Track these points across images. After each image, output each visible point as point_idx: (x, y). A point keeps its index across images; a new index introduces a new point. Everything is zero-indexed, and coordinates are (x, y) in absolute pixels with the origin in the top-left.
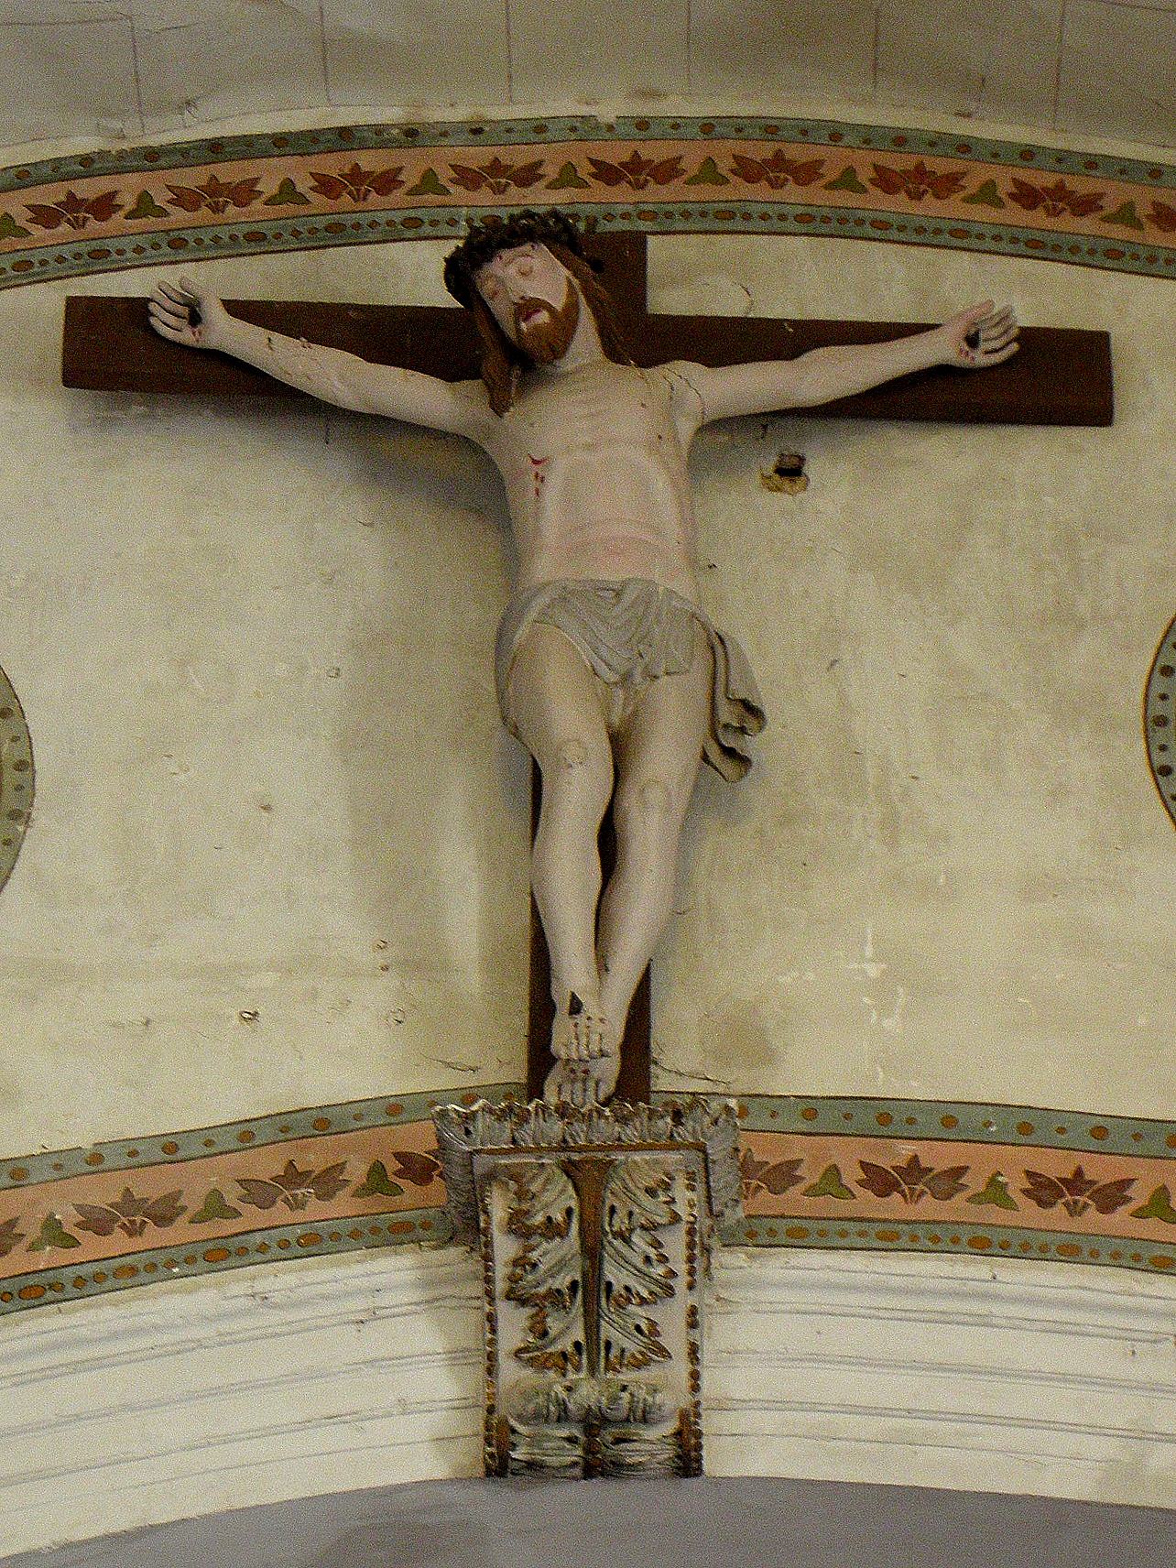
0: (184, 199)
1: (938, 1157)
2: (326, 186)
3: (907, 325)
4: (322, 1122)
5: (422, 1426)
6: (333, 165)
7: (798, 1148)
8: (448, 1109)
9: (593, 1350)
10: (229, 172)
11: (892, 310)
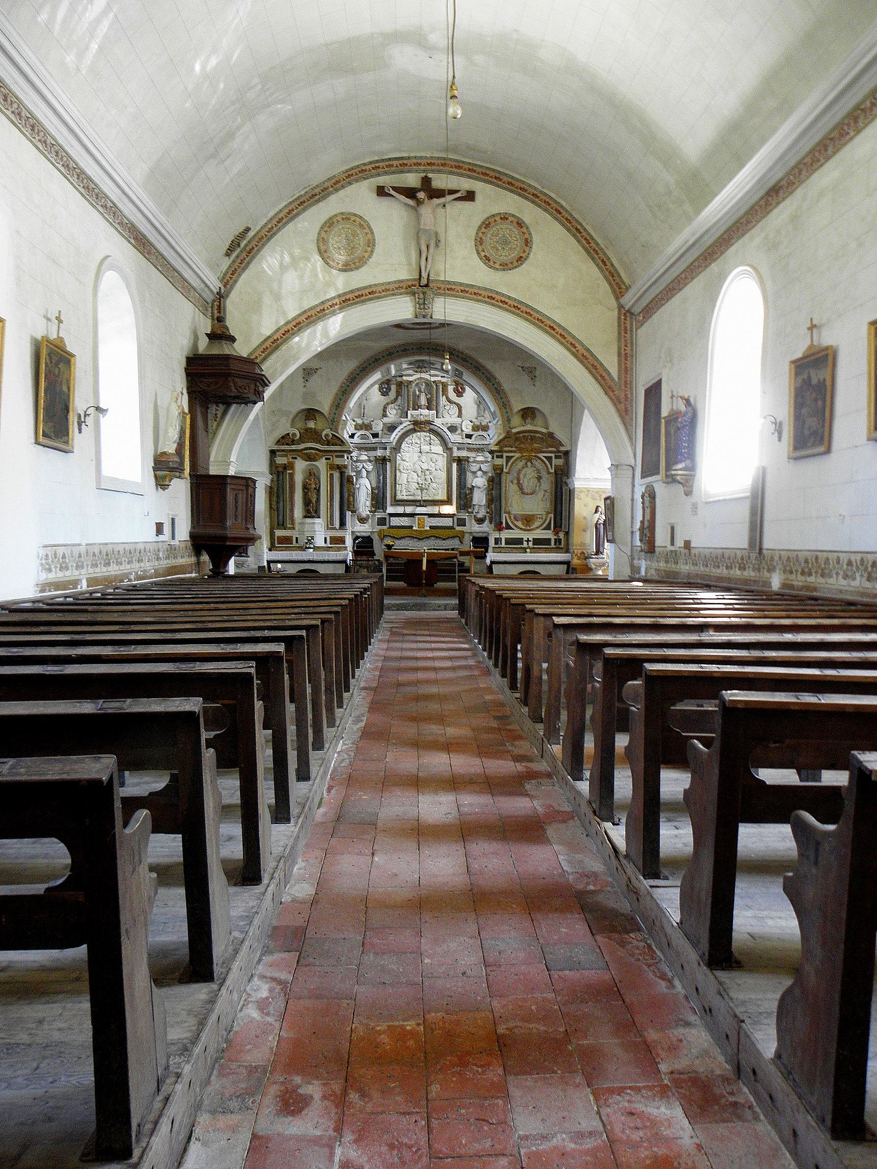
0: (387, 166)
1: (453, 287)
2: (401, 165)
3: (466, 200)
4: (402, 281)
5: (410, 313)
6: (401, 162)
7: (441, 285)
8: (188, 1062)
9: (424, 308)
10: (391, 163)
11: (455, 188)
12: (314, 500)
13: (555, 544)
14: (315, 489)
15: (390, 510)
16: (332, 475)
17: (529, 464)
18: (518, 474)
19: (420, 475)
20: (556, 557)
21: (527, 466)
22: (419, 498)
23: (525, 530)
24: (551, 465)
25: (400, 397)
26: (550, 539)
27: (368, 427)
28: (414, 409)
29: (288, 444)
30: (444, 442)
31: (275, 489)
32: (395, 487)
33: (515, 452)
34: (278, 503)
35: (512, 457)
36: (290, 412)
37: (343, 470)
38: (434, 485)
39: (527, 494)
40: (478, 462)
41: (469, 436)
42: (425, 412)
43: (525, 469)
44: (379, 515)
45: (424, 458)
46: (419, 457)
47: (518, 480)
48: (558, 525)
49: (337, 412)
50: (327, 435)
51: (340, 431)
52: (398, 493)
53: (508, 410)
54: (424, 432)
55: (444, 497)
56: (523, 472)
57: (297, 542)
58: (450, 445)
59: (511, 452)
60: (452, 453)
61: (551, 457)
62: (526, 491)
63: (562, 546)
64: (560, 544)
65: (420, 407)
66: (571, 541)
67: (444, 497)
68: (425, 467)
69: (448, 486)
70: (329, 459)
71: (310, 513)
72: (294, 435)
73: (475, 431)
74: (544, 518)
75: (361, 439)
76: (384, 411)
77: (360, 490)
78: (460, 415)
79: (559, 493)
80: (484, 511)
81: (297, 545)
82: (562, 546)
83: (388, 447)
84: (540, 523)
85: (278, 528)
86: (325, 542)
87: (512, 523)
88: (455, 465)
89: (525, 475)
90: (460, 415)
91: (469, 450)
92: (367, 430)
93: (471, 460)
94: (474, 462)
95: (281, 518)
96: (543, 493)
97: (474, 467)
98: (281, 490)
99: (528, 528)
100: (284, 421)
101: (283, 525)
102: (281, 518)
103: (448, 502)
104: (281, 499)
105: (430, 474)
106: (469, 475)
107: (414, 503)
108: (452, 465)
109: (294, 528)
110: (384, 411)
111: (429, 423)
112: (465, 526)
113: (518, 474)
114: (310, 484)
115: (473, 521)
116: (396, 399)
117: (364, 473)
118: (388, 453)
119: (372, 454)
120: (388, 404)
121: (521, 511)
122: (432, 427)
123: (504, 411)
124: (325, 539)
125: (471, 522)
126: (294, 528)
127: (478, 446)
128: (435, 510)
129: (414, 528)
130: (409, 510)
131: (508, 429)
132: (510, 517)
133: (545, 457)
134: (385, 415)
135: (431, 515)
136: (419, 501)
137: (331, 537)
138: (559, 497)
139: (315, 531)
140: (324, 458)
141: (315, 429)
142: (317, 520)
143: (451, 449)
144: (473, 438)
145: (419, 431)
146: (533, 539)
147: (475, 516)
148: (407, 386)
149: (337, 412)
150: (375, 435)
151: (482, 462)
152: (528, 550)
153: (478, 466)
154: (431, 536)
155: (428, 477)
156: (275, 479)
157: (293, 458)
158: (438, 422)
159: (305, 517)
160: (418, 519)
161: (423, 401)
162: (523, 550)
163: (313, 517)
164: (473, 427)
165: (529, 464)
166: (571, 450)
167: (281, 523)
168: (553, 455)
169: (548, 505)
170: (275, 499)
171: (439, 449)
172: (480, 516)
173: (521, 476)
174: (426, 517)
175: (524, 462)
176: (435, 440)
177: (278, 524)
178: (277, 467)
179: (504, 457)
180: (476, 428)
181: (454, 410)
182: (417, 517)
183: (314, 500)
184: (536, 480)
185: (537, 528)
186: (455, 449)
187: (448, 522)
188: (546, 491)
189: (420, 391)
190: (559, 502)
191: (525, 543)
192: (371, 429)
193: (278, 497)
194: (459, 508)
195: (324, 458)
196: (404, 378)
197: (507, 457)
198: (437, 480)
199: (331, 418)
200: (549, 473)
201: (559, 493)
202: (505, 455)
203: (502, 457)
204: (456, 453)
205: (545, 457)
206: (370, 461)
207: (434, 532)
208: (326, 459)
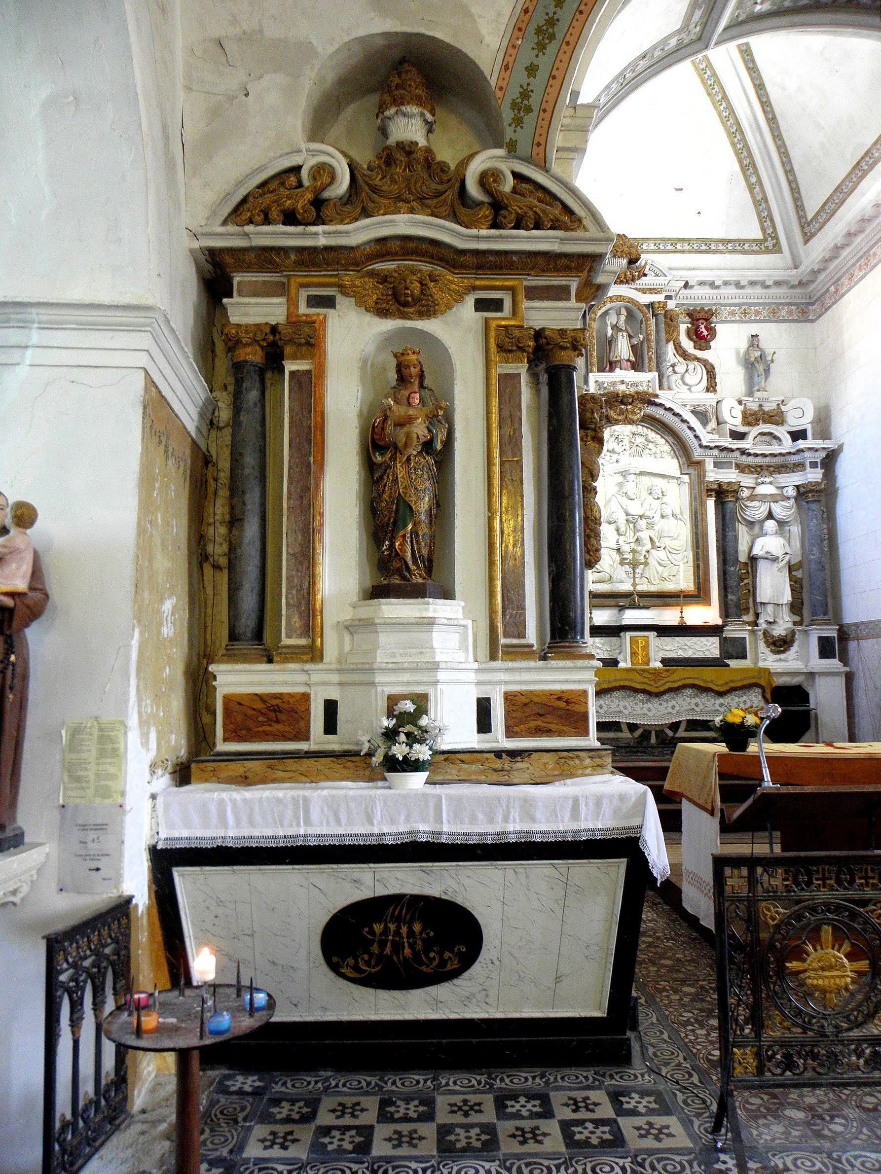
12: (423, 505)
14: (428, 446)
16: (509, 382)
19: (622, 529)
22: (626, 587)
28: (601, 370)
29: (290, 218)
30: (681, 448)
31: (225, 464)
34: (235, 521)
36: (305, 50)
37: (563, 357)
38: (661, 555)
40: (763, 498)
41: (738, 436)
42: (631, 376)
45: (630, 488)
46: (620, 485)
49: (544, 62)
50: (486, 179)
51: (556, 168)
54: (631, 422)
55: (685, 582)
57: (330, 727)
58: (697, 454)
60: (701, 475)
65: (612, 366)
67: (685, 582)
68: (635, 509)
69: (696, 558)
70: (496, 305)
71: (403, 570)
72: (324, 172)
73: (749, 424)
78: (711, 387)
80: (787, 618)
81: (333, 743)
85: (231, 657)
86: (484, 724)
88: (711, 503)
90: (711, 387)
91: (741, 468)
93: (746, 493)
94: (752, 498)
95: (248, 601)
97: (757, 511)
98: (250, 460)
100: (273, 98)
101: (258, 635)
102: (248, 601)
103: (700, 595)
104: (252, 499)
105: (650, 526)
106: (742, 531)
107: (612, 601)
108: (703, 504)
109: (314, 654)
111: (648, 400)
112: (744, 657)
114: (405, 422)
115: (762, 646)
122: (651, 410)
124: (484, 708)
125: (756, 647)
126: (314, 654)
127: (759, 460)
128: (669, 616)
129: (622, 665)
135: (664, 631)
136: (627, 595)
137: (509, 698)
139: (434, 667)
140: (470, 301)
141: (428, 150)
142: (437, 608)
143: (699, 464)
144: (751, 437)
145: (617, 422)
147: (766, 633)
149: (544, 62)
151: (774, 499)
153: (763, 510)
154: (684, 687)
155: (644, 535)
156: (224, 414)
157: (316, 301)
158: (664, 397)
159: (378, 592)
161: (623, 349)
163: (418, 592)
164: (744, 414)
167: (247, 623)
170: (219, 509)
171: (671, 465)
172: (779, 631)
174: (652, 635)
176: (661, 444)
177: (233, 637)
178: (233, 344)
180: (751, 418)
181: (697, 375)
182: (629, 635)
183: (423, 505)
186: (709, 465)
187: (709, 647)
193: (236, 490)
194: (726, 611)
195: (470, 301)
198: (666, 542)
199: (514, 93)
204: (713, 475)
207: (681, 675)
208: (481, 305)
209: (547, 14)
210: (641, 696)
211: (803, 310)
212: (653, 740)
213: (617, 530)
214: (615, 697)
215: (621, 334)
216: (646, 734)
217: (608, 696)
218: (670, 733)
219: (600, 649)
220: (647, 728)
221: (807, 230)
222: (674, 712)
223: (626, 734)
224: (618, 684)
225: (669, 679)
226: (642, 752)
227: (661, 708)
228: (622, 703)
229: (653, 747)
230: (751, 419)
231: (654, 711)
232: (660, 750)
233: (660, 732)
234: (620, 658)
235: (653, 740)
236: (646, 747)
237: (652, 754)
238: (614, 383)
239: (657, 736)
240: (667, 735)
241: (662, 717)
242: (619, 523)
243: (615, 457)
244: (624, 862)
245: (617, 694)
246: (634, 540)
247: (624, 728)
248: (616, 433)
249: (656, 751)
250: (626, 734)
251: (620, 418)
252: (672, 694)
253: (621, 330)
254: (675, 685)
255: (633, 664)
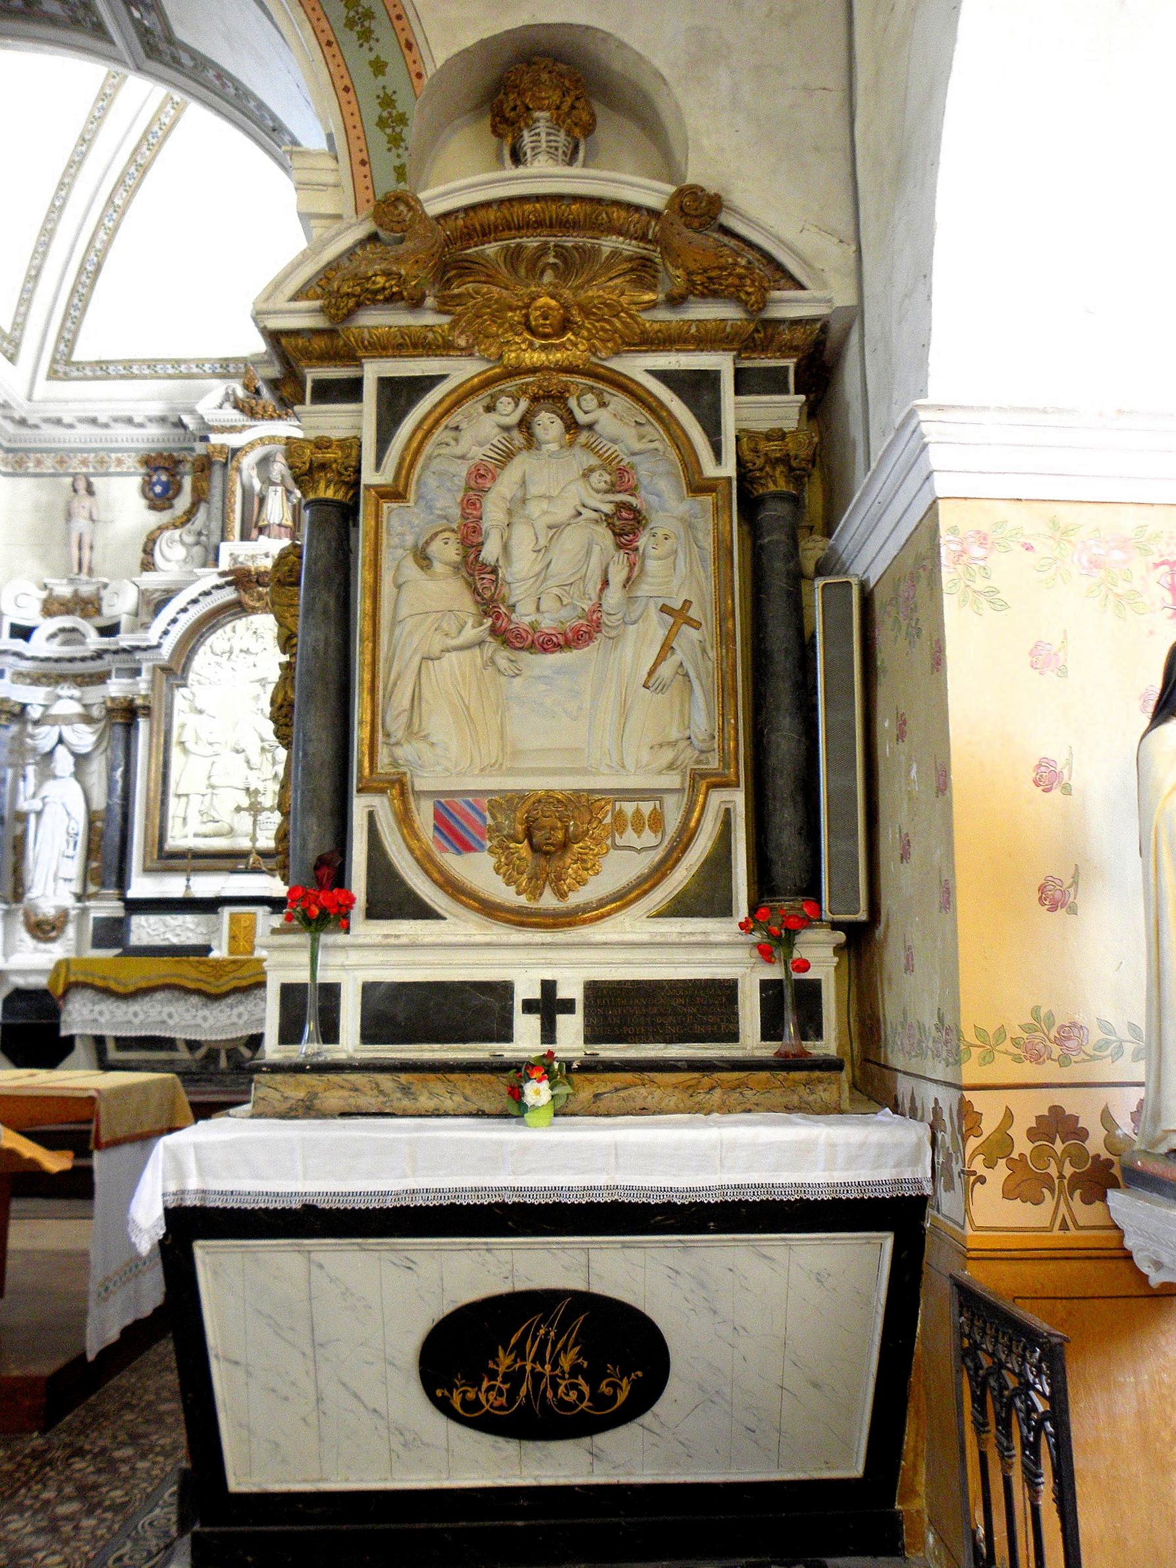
13: (770, 1030)
15: (141, 886)
17: (548, 425)
18: (473, 498)
20: (805, 1149)
21: (531, 442)
22: (244, 844)
23: (521, 919)
24: (713, 430)
25: (203, 508)
26: (726, 991)
27: (87, 606)
28: (245, 536)
32: (164, 803)
33: (444, 348)
35: (423, 385)
39: (548, 645)
43: (521, 464)
44: (107, 907)
47: (471, 540)
48: (787, 869)
52: (170, 832)
53: (386, 47)
56: (505, 485)
59: (418, 345)
61: (710, 379)
62: (524, 616)
63: (828, 1045)
64: (811, 1025)
66: (890, 1011)
74: (673, 822)
75: (65, 643)
76: (148, 551)
77: (45, 818)
79: (779, 637)
82: (828, 1045)
83: (145, 667)
84: (641, 865)
87: (427, 863)
89: (517, 506)
92: (85, 616)
96: (656, 628)
99: (549, 901)
107: (228, 863)
110: (148, 551)
113: (473, 498)
116: (190, 514)
117: (64, 762)
118: (142, 684)
119: (95, 694)
120: (161, 529)
121: (494, 768)
123: (359, 59)
129: (215, 954)
130: (206, 886)
131: (387, 184)
132: (404, 819)
133: (663, 376)
134: (148, 565)
138: (783, 663)
146: (594, 989)
148: (225, 465)
150: (109, 631)
152: (537, 1092)
160: (234, 918)
162: (494, 1091)
165: (548, 425)
166: (856, 313)
168: (722, 362)
169: (702, 721)
173: (493, 512)
175: (509, 411)
179: (370, 390)
182: (226, 912)
184: (605, 537)
185: (623, 899)
188: (679, 616)
189: (268, 481)
190: (782, 692)
191: (526, 1028)
192: (99, 611)
196: (215, 439)
197: (385, 383)
200: (699, 486)
201: (779, 637)
202: (372, 371)
203: (351, 390)
205: (663, 376)
206: (87, 719)
209: (377, 40)
210: (195, 1000)
211: (20, 466)
212: (223, 1063)
213: (248, 762)
214: (157, 1001)
215: (272, 488)
216: (212, 1055)
217: (147, 999)
218: (247, 1053)
219: (192, 930)
220: (213, 1045)
221: (61, 375)
222: (241, 1022)
223: (183, 1054)
224: (160, 982)
225: (237, 974)
226: (206, 1080)
227: (188, 1016)
228: (166, 1010)
229: (223, 1073)
230: (55, 607)
231: (211, 1021)
232: (233, 1077)
233: (232, 1053)
234: (214, 944)
235: (223, 1063)
236: (212, 1074)
237: (220, 1082)
238: (253, 557)
239: (228, 1058)
240: (242, 1056)
241: (223, 1029)
242: (248, 752)
243: (250, 659)
244: (888, 1240)
245: (159, 996)
246: (271, 776)
247: (181, 1046)
248: (254, 626)
249: (228, 1079)
250: (183, 1054)
251: (257, 605)
252: (238, 996)
253: (274, 484)
254: (244, 983)
255: (231, 952)
